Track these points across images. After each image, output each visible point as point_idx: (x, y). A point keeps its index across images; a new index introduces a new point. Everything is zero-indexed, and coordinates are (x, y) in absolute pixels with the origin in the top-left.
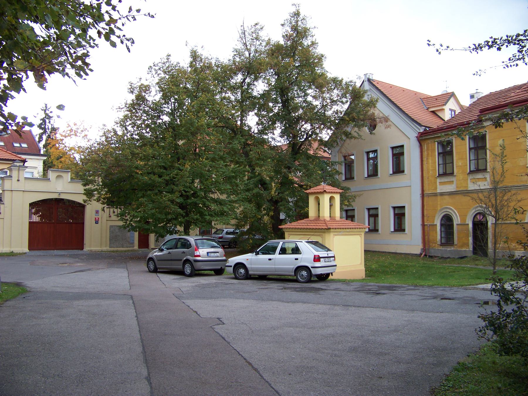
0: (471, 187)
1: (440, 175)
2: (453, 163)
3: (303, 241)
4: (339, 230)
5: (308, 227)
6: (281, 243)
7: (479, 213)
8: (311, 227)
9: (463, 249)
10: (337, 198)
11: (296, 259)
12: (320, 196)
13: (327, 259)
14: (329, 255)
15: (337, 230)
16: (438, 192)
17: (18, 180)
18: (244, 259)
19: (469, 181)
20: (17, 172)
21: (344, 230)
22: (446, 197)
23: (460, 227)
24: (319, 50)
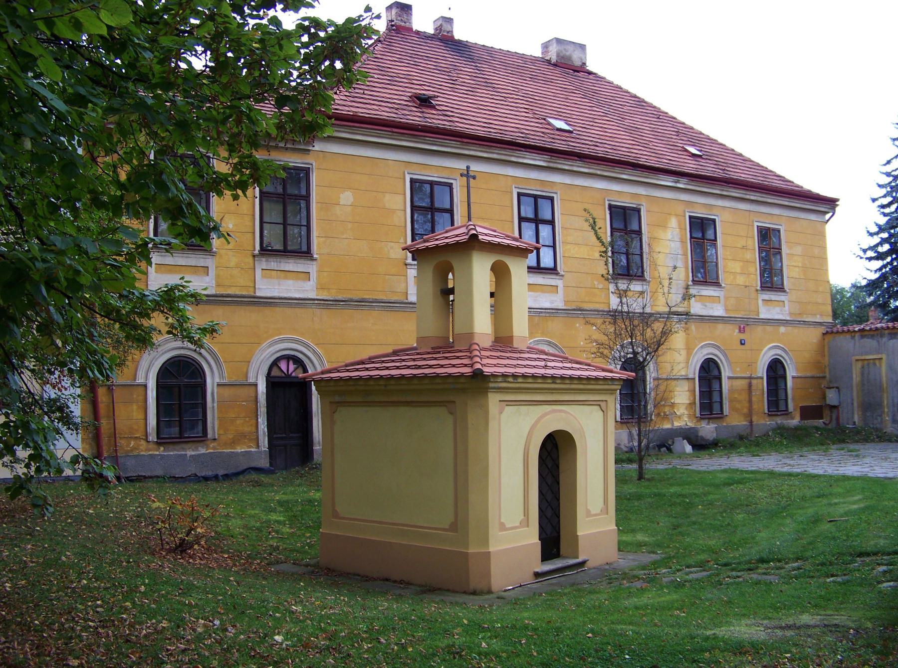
0: (266, 288)
7: (288, 358)
9: (239, 450)
19: (760, 302)
23: (227, 392)
24: (340, 21)
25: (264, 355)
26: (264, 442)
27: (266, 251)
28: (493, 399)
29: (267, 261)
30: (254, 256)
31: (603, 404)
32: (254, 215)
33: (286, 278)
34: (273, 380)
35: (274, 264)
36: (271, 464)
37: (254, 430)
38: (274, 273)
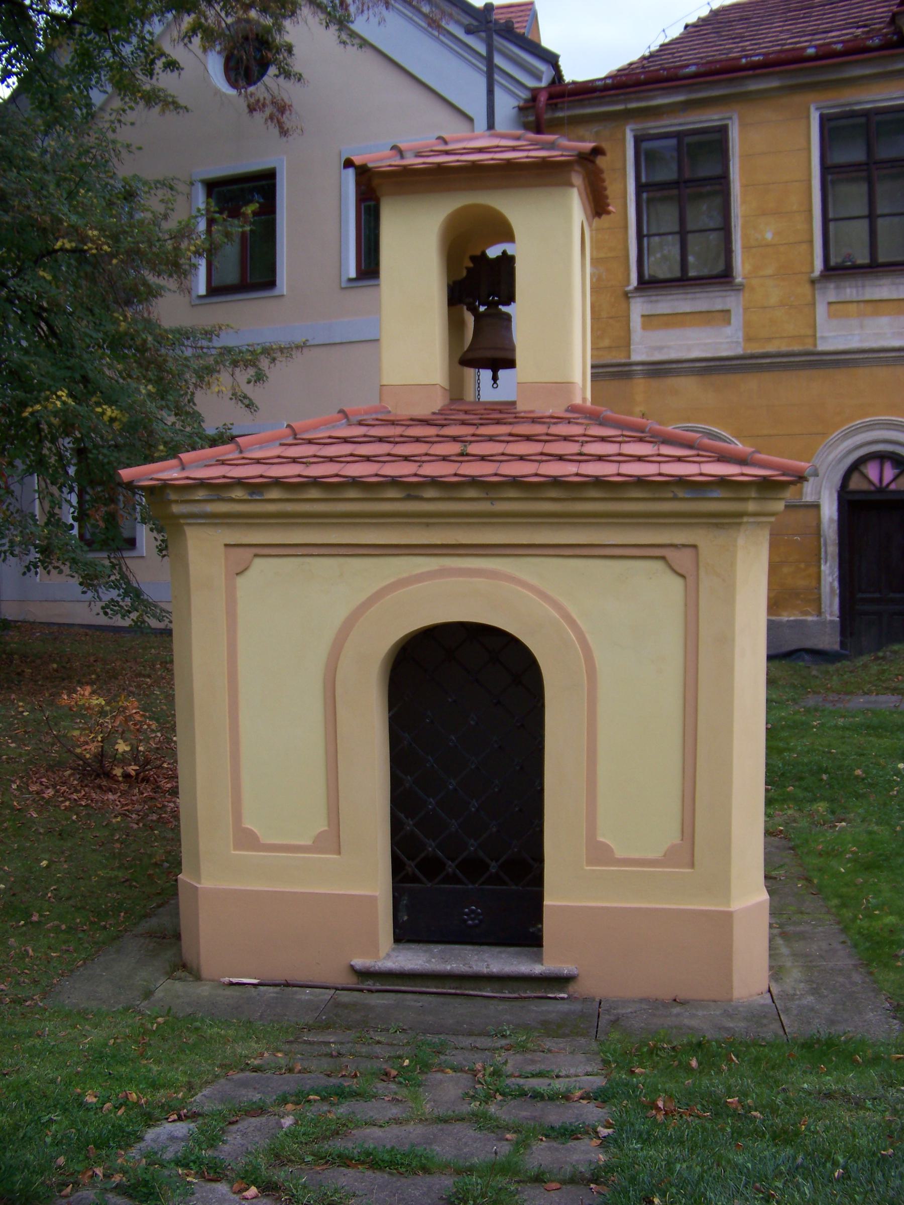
0: (836, 335)
1: (647, 284)
2: (726, 230)
7: (881, 457)
16: (635, 358)
22: (688, 385)
25: (831, 457)
26: (831, 608)
27: (836, 271)
28: (204, 549)
29: (837, 288)
30: (813, 282)
31: (681, 558)
32: (810, 211)
33: (876, 314)
34: (850, 497)
35: (850, 291)
36: (842, 644)
37: (814, 583)
38: (853, 308)
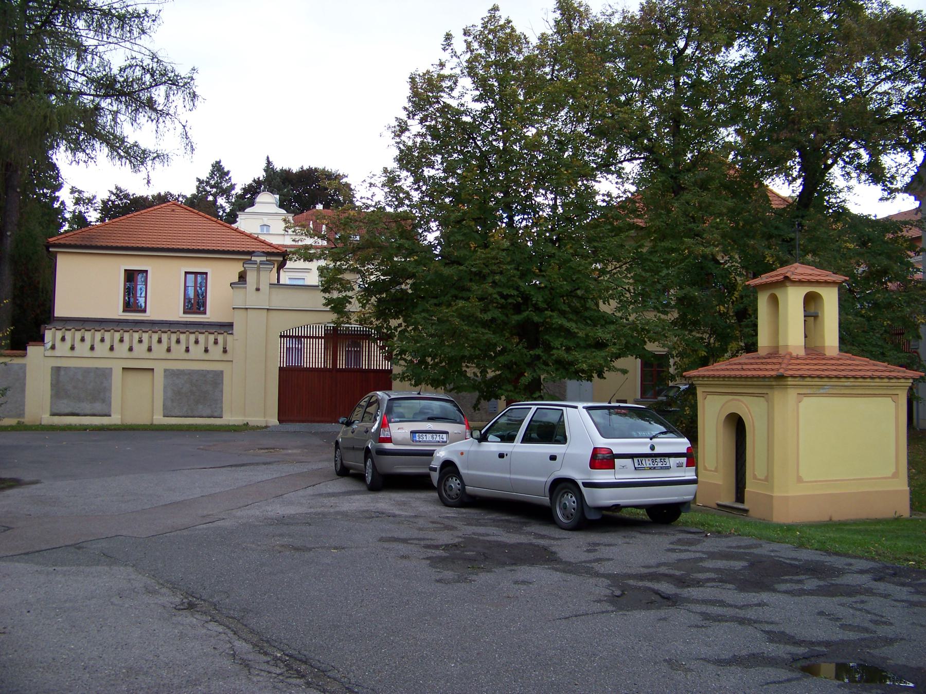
3: (580, 405)
4: (817, 382)
5: (743, 373)
6: (534, 408)
8: (749, 373)
10: (830, 299)
11: (553, 458)
12: (779, 293)
13: (647, 462)
14: (658, 450)
15: (808, 382)
17: (258, 290)
18: (455, 452)
20: (255, 273)
21: (834, 382)
